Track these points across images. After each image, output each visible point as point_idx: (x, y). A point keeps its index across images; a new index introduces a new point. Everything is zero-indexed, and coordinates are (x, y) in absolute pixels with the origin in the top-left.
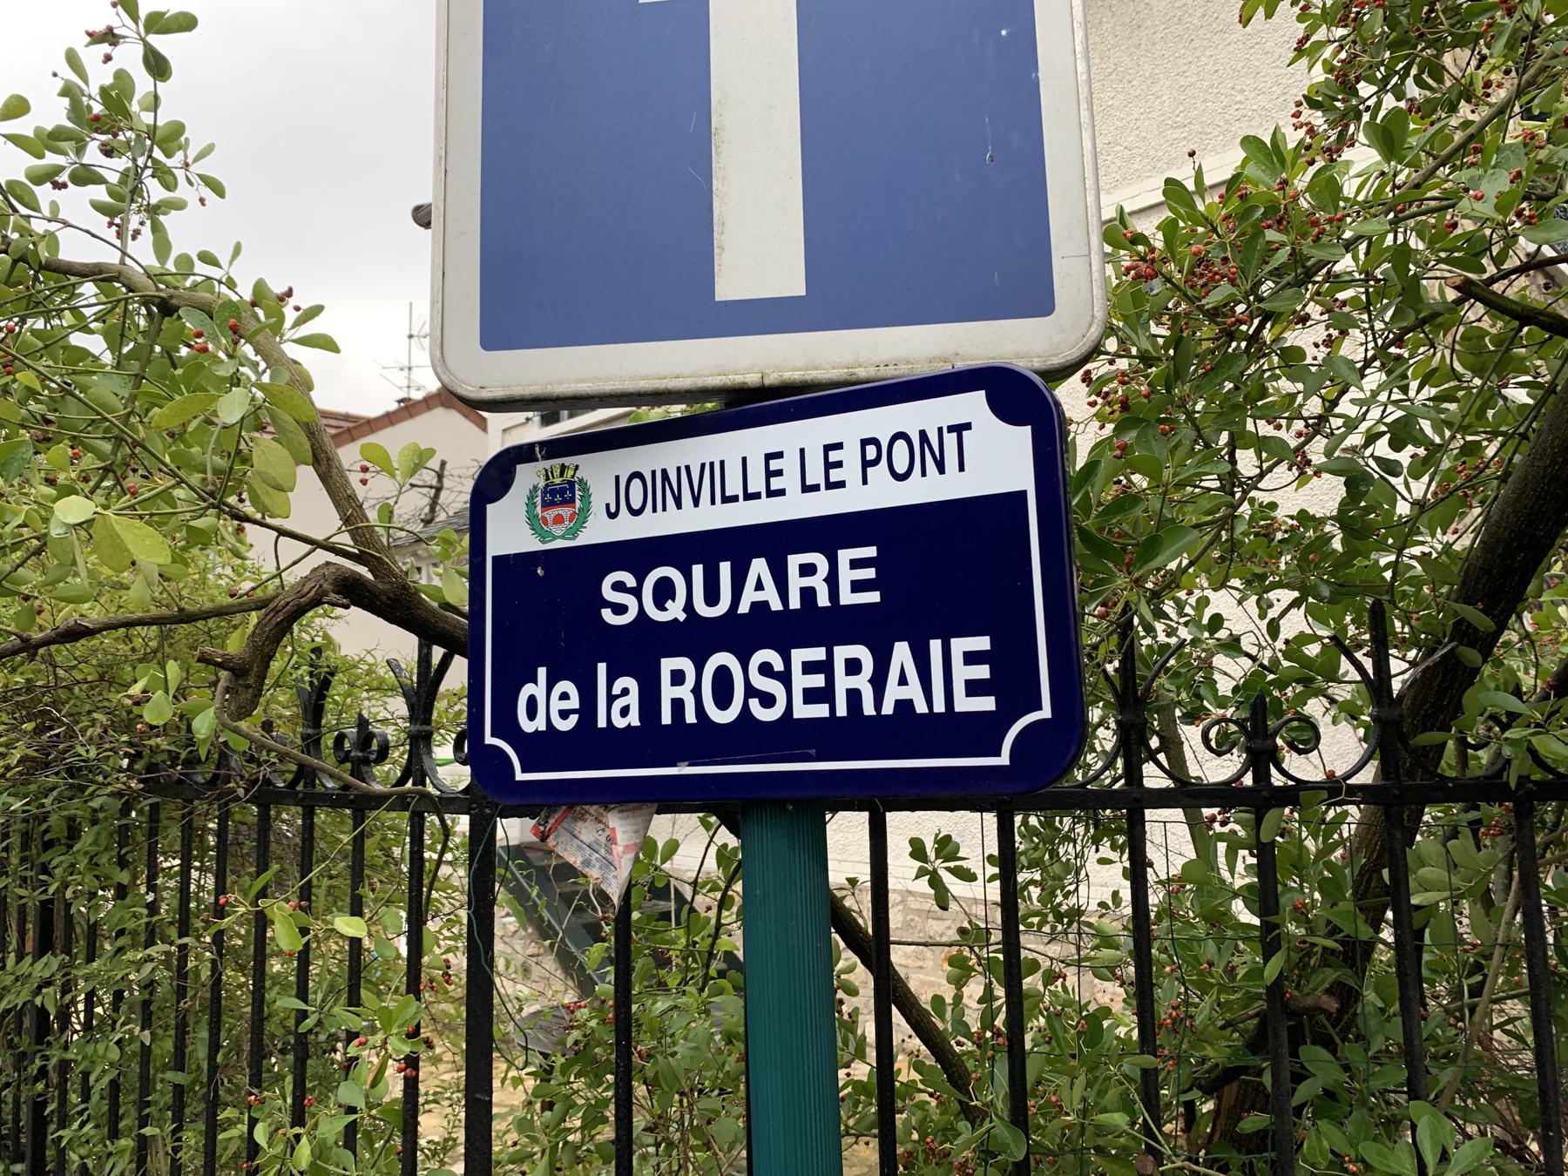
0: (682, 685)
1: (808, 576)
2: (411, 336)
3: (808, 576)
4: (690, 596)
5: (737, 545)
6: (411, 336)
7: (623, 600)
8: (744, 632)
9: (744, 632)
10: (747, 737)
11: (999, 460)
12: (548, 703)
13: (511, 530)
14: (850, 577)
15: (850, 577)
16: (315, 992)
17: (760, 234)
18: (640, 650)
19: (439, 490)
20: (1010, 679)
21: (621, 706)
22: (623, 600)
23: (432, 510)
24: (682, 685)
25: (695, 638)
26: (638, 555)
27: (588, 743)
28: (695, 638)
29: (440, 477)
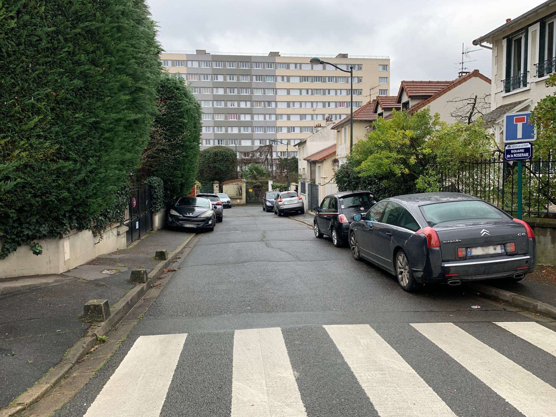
0: (515, 155)
1: (521, 151)
2: (463, 53)
3: (521, 151)
4: (515, 151)
5: (518, 149)
6: (463, 53)
7: (512, 151)
8: (518, 153)
9: (518, 153)
10: (518, 157)
11: (529, 146)
12: (508, 156)
13: (507, 148)
14: (523, 151)
15: (523, 151)
16: (402, 280)
17: (519, 135)
18: (513, 154)
19: (475, 104)
20: (529, 155)
21: (512, 156)
22: (512, 151)
23: (473, 109)
24: (515, 155)
25: (516, 153)
26: (513, 149)
27: (510, 158)
28: (516, 153)
29: (475, 101)
